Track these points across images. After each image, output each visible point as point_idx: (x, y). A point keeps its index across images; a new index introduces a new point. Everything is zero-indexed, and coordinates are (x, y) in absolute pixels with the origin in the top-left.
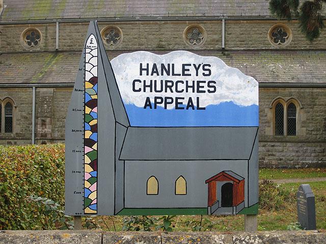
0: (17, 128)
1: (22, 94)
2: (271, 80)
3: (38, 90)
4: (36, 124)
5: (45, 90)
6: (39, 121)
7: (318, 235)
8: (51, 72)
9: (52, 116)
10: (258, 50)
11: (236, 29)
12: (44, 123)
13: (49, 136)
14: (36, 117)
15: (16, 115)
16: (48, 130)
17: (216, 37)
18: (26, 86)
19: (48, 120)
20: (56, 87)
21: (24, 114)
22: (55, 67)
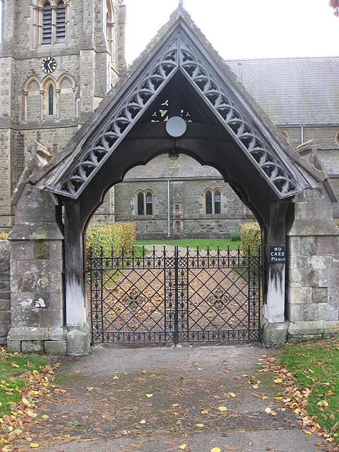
0: (156, 211)
1: (160, 186)
2: (297, 218)
3: (171, 182)
4: (171, 208)
5: (177, 182)
6: (174, 206)
7: (91, 69)
8: (178, 169)
9: (183, 203)
10: (328, 150)
11: (311, 133)
12: (177, 207)
13: (181, 217)
14: (171, 203)
15: (155, 202)
16: (180, 212)
17: (296, 140)
18: (162, 180)
19: (180, 205)
20: (185, 180)
21: (161, 201)
22: (179, 165)
